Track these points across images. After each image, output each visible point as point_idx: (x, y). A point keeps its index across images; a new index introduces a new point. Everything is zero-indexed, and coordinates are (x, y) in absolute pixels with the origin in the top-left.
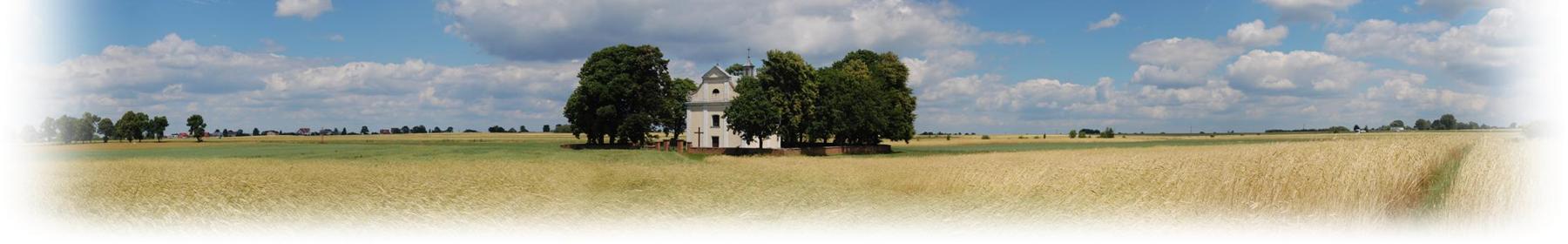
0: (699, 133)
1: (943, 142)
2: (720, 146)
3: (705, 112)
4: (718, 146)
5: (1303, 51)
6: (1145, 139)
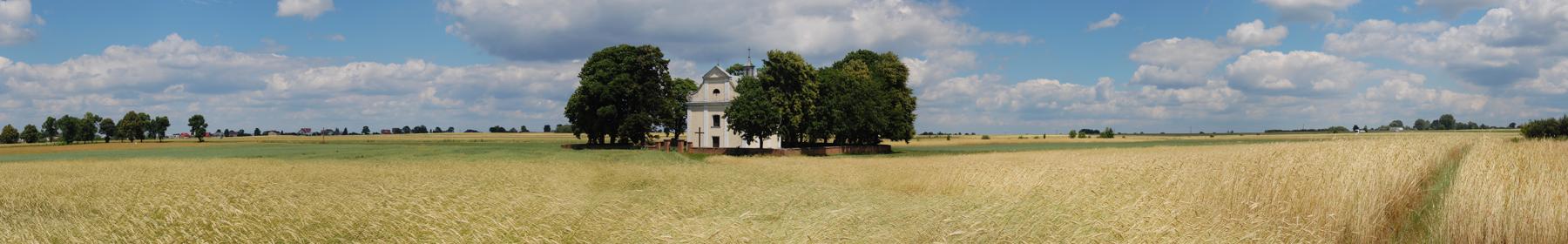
3: (706, 112)
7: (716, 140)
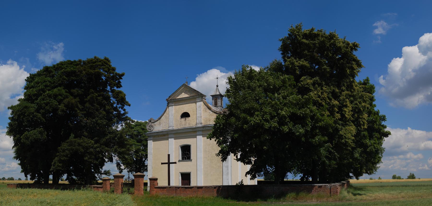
0: (169, 163)
1: (192, 90)
2: (193, 184)
3: (172, 141)
4: (189, 183)
5: (30, 183)
6: (207, 126)
7: (186, 177)
